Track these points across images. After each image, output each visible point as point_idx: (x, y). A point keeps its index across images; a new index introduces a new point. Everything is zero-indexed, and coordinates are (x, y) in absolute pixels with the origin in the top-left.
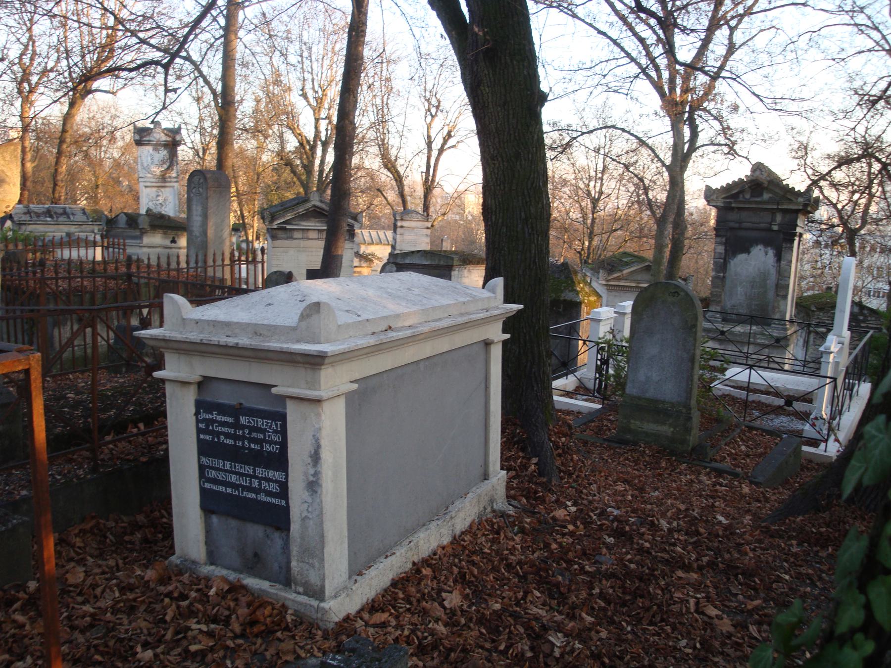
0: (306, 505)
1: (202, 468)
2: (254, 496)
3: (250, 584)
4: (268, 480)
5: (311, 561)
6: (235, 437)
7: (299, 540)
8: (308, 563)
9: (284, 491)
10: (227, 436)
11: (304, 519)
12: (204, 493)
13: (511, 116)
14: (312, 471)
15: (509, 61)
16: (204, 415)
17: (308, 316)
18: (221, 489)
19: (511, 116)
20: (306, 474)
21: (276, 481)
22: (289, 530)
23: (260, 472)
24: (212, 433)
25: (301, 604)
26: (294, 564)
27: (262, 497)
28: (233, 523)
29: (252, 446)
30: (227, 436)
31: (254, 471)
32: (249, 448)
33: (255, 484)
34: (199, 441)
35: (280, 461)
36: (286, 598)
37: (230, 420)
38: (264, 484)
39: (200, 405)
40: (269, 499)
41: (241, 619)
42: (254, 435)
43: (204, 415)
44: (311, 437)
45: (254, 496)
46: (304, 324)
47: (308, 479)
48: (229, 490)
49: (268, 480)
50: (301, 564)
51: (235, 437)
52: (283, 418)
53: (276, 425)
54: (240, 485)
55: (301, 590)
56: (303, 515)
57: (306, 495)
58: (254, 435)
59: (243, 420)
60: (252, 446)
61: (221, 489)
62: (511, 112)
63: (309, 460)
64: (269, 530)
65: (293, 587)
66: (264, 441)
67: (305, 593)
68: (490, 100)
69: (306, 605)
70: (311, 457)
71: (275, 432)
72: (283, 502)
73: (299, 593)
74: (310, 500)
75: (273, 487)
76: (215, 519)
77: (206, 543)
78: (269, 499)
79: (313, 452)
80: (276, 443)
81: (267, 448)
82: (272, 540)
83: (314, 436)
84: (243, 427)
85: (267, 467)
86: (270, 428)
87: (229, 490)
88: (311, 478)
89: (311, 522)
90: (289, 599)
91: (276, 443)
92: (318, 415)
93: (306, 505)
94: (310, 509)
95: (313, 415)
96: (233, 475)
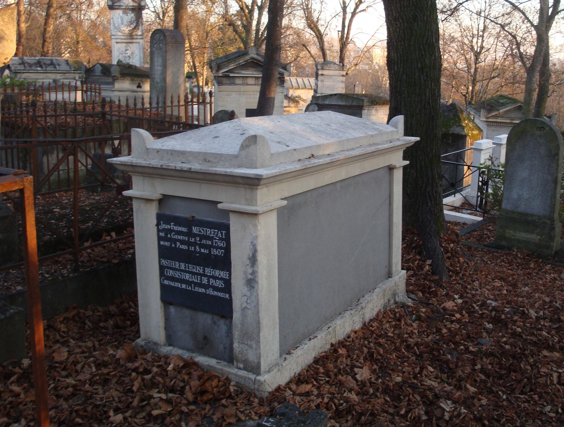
0: (245, 298)
1: (162, 268)
2: (203, 290)
3: (201, 361)
4: (215, 278)
6: (188, 243)
7: (240, 326)
8: (247, 344)
9: (228, 287)
10: (182, 242)
14: (250, 271)
16: (163, 226)
17: (248, 146)
21: (221, 279)
23: (208, 271)
24: (170, 240)
25: (241, 377)
26: (236, 345)
27: (211, 292)
28: (187, 312)
29: (202, 250)
30: (182, 242)
31: (204, 271)
32: (200, 252)
33: (205, 281)
35: (225, 262)
36: (229, 373)
38: (212, 281)
39: (161, 218)
40: (216, 293)
41: (193, 389)
42: (204, 242)
43: (163, 226)
44: (250, 244)
45: (203, 290)
46: (243, 153)
47: (247, 277)
48: (184, 286)
49: (215, 278)
50: (241, 345)
51: (188, 243)
52: (227, 228)
53: (222, 233)
54: (193, 282)
55: (241, 366)
57: (245, 290)
58: (204, 242)
59: (195, 230)
60: (202, 250)
61: (178, 285)
63: (248, 262)
65: (235, 364)
67: (245, 369)
69: (245, 378)
70: (249, 259)
72: (227, 296)
73: (240, 369)
74: (248, 294)
75: (219, 284)
76: (172, 309)
77: (166, 328)
78: (216, 293)
79: (251, 255)
81: (214, 252)
82: (218, 326)
83: (252, 242)
84: (195, 235)
86: (216, 236)
87: (184, 286)
88: (250, 277)
89: (250, 312)
90: (232, 373)
91: (221, 248)
93: (245, 298)
94: (249, 301)
96: (187, 274)
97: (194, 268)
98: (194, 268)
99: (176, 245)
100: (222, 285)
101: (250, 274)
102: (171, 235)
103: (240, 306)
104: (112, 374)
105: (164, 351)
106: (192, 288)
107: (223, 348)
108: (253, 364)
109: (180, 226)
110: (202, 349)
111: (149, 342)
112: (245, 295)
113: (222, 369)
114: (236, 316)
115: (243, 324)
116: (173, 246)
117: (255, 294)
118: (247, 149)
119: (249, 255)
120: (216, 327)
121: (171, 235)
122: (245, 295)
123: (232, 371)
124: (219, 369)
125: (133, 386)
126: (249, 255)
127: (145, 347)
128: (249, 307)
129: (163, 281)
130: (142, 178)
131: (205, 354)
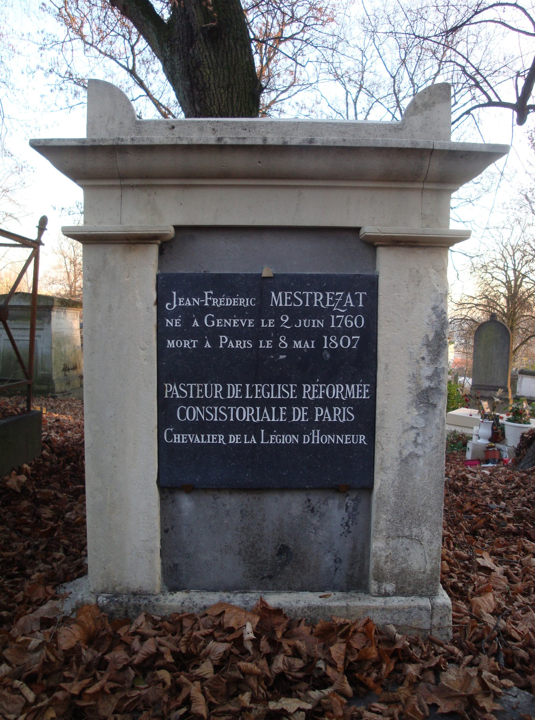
0: (412, 434)
1: (166, 408)
2: (294, 438)
3: (284, 604)
4: (328, 403)
5: (415, 531)
6: (257, 334)
7: (393, 499)
8: (409, 537)
9: (366, 416)
10: (234, 334)
11: (405, 461)
12: (167, 453)
13: (235, 99)
14: (427, 371)
15: (232, 44)
16: (178, 302)
17: (427, 106)
18: (212, 438)
19: (235, 99)
20: (414, 378)
21: (349, 402)
22: (369, 488)
23: (310, 391)
24: (200, 334)
25: (399, 610)
26: (378, 545)
27: (316, 438)
28: (232, 502)
29: (297, 344)
30: (234, 334)
31: (299, 391)
32: (290, 351)
33: (300, 415)
34: (162, 351)
35: (362, 362)
36: (367, 610)
37: (244, 302)
38: (320, 413)
39: (165, 286)
40: (329, 438)
41: (340, 665)
42: (303, 323)
43: (178, 302)
44: (430, 311)
45: (294, 438)
46: (417, 120)
47: (418, 384)
48: (234, 439)
49: (328, 403)
50: (392, 543)
51: (257, 334)
52: (371, 285)
53: (355, 299)
54: (265, 425)
55: (390, 587)
56: (406, 453)
57: (413, 416)
58: (303, 323)
59: (277, 299)
60: (297, 344)
61: (212, 438)
62: (235, 95)
63: (424, 353)
64: (315, 498)
65: (374, 586)
66: (327, 331)
67: (400, 592)
68: (211, 82)
69: (409, 611)
70: (428, 345)
71: (352, 311)
72: (362, 439)
73: (387, 595)
74: (421, 423)
75: (341, 415)
76: (186, 503)
77: (163, 553)
78: (329, 438)
79: (431, 336)
80: (351, 332)
81: (331, 343)
82: (322, 515)
83: (434, 308)
84: (278, 311)
85: (330, 378)
86: (340, 306)
87: (234, 439)
88: (426, 384)
89: (421, 462)
90: (376, 609)
91: (351, 332)
92: (442, 271)
93: (412, 434)
94: (420, 440)
95: (432, 270)
96: (241, 409)
97: (268, 389)
98: (268, 389)
99: (215, 342)
100: (347, 415)
101: (429, 378)
102: (201, 322)
103: (397, 455)
104: (88, 691)
105: (174, 604)
106: (258, 439)
107: (331, 563)
108: (421, 576)
109: (232, 296)
110: (270, 577)
111: (117, 595)
112: (413, 428)
113: (347, 608)
114: (384, 479)
115: (401, 495)
116: (208, 345)
117: (438, 420)
118: (426, 113)
119: (427, 336)
120: (315, 521)
121: (201, 322)
122: (413, 428)
123: (374, 604)
124: (340, 608)
125: (188, 702)
126: (427, 336)
127: (113, 608)
128: (420, 452)
129: (170, 437)
130: (117, 193)
131: (278, 589)
